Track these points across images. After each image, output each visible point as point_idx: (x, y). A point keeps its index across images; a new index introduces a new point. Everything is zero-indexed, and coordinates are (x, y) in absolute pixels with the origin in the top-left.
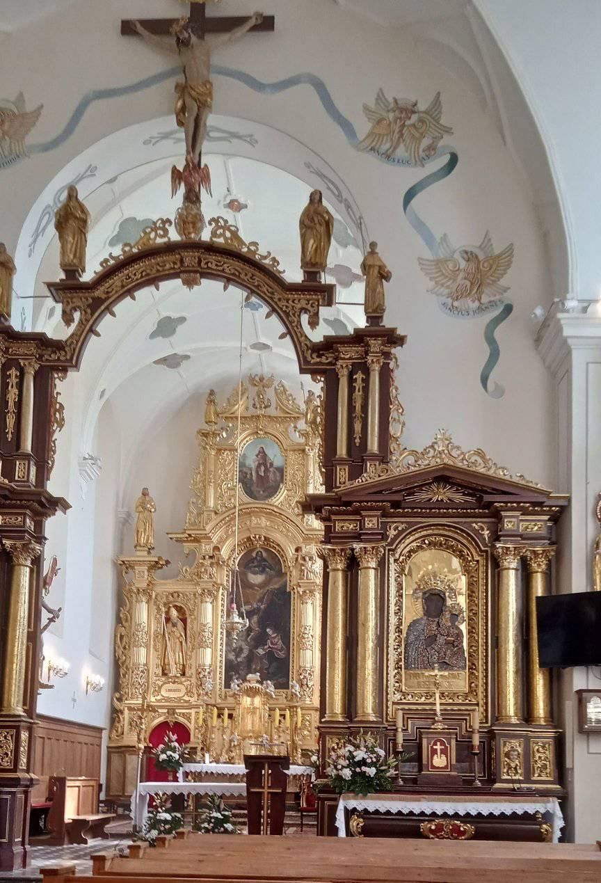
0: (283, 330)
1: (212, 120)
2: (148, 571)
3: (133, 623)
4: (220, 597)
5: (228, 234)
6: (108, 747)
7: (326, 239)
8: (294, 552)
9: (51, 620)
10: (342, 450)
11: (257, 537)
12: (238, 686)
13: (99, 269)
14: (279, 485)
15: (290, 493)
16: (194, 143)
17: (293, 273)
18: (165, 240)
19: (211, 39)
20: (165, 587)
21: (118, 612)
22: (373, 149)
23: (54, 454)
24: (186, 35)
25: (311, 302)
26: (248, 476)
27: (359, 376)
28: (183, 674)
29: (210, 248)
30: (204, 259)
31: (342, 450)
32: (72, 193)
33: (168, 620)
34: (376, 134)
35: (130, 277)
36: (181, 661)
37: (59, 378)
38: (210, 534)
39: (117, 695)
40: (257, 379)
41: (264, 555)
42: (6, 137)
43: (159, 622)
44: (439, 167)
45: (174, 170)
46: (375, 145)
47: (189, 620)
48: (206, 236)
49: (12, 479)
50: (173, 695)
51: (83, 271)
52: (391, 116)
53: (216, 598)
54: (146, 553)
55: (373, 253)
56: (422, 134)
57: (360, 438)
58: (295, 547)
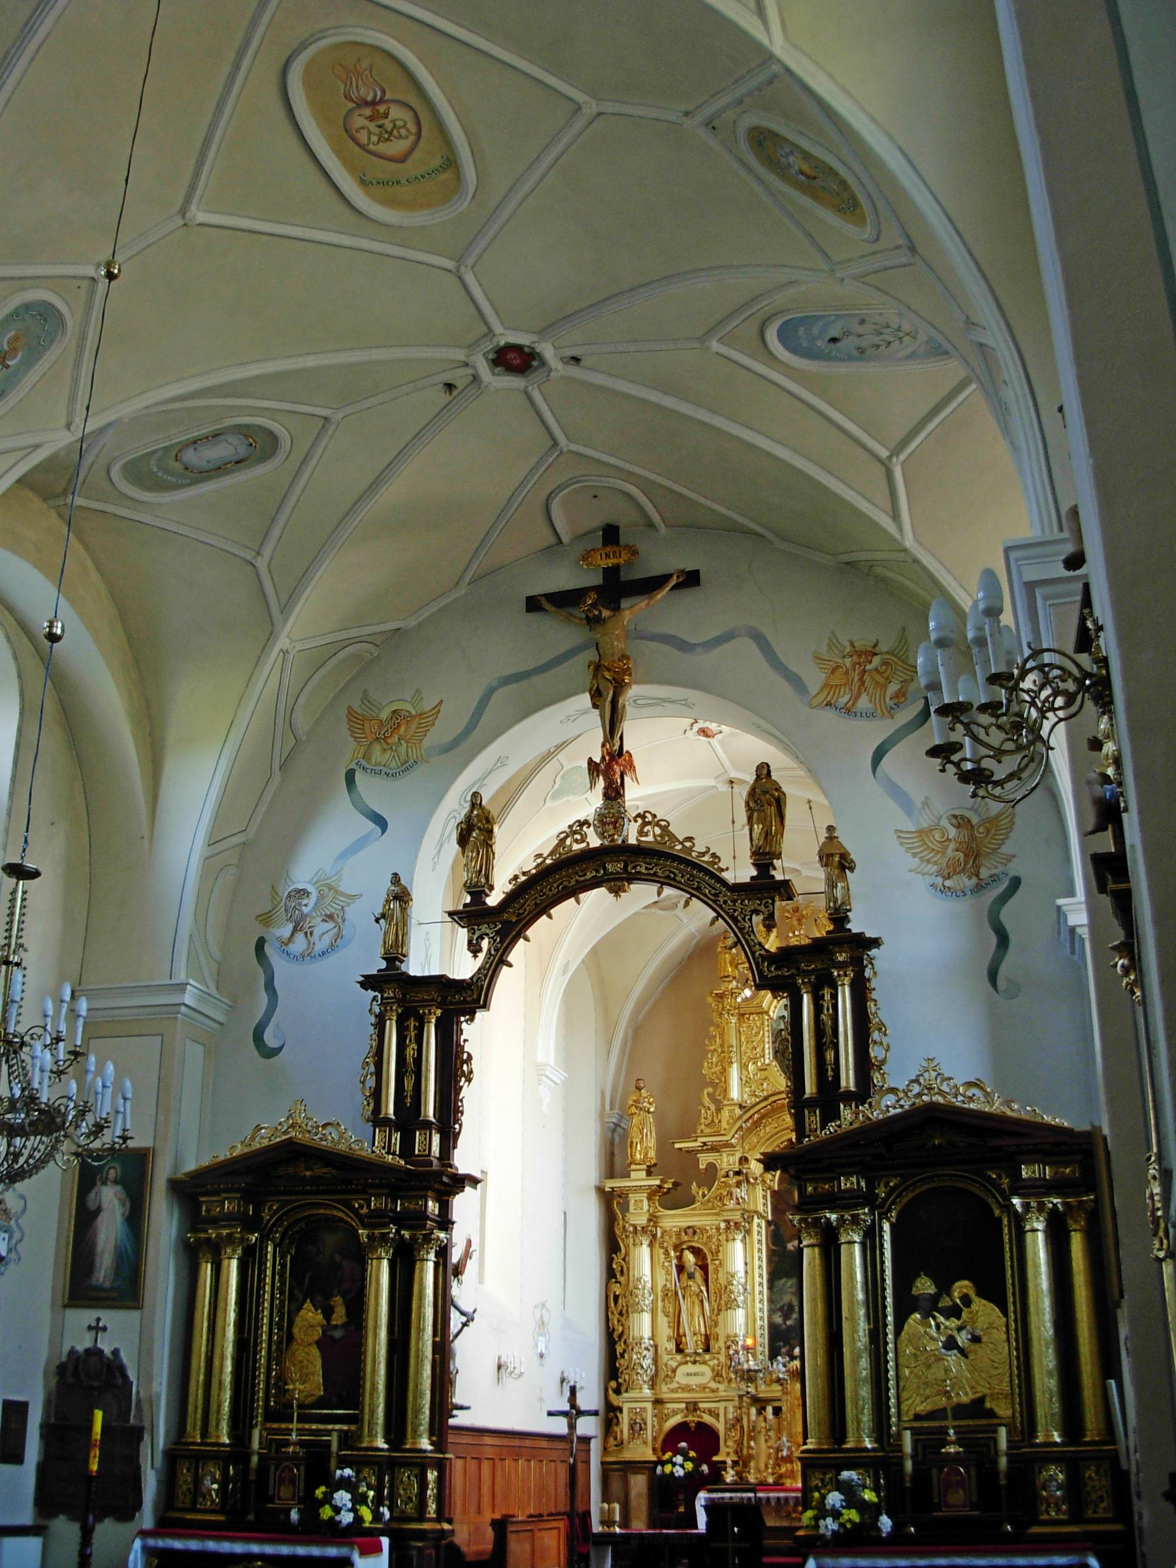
1: (634, 691)
2: (649, 1199)
3: (631, 1278)
4: (755, 1228)
5: (658, 831)
6: (603, 1463)
7: (778, 819)
9: (465, 1325)
10: (810, 1088)
12: (785, 1366)
13: (509, 888)
16: (612, 725)
17: (741, 871)
18: (583, 845)
20: (674, 1221)
21: (610, 1262)
22: (829, 704)
27: (412, 1023)
28: (707, 1350)
31: (810, 1088)
33: (681, 1268)
36: (703, 1329)
37: (466, 1021)
39: (613, 1384)
43: (668, 1273)
44: (915, 713)
45: (590, 761)
47: (711, 1268)
50: (693, 1381)
51: (491, 888)
52: (848, 661)
53: (748, 1232)
56: (887, 679)
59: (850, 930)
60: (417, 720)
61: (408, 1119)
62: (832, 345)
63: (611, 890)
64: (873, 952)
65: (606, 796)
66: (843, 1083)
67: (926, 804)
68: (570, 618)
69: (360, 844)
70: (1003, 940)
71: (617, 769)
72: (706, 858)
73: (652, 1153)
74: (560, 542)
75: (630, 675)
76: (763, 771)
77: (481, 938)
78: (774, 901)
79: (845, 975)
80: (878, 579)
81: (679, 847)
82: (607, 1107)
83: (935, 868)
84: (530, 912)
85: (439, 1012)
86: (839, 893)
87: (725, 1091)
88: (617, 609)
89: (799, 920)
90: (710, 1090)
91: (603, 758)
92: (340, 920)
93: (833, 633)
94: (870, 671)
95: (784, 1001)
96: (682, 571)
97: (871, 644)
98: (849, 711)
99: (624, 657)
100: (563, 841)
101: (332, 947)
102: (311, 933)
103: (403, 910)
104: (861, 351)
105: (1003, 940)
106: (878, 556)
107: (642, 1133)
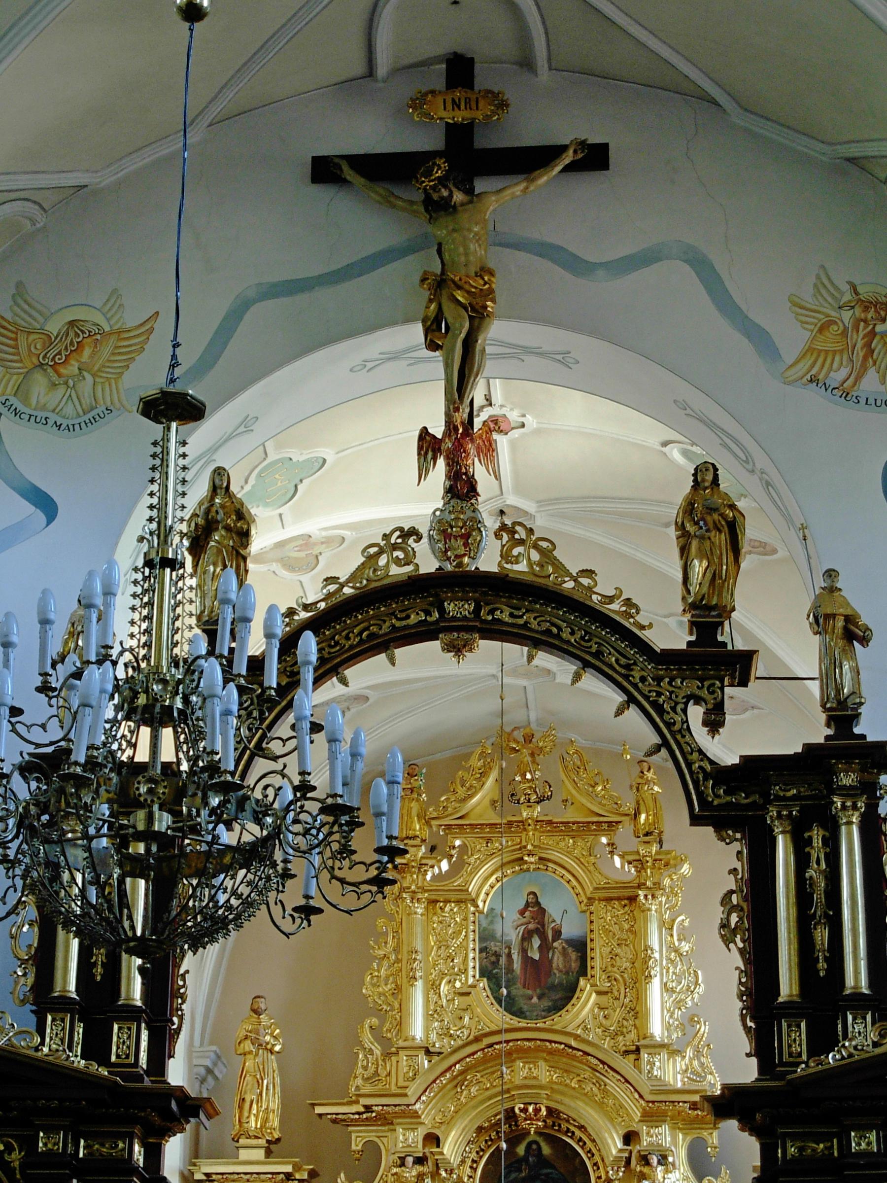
0: (619, 698)
1: (497, 332)
5: (535, 556)
7: (731, 558)
8: (620, 1145)
10: (788, 985)
11: (531, 1109)
14: (578, 981)
15: (604, 998)
17: (670, 632)
18: (410, 568)
23: (183, 1002)
24: (445, 193)
25: (706, 684)
26: (503, 961)
27: (817, 835)
30: (487, 604)
31: (788, 985)
34: (820, 351)
35: (337, 643)
38: (417, 1106)
40: (519, 735)
41: (546, 1150)
42: (85, 373)
45: (424, 434)
46: (819, 373)
48: (488, 560)
49: (104, 1060)
54: (260, 1154)
55: (832, 590)
57: (826, 959)
58: (622, 1132)
61: (98, 1003)
65: (452, 492)
66: (850, 981)
68: (388, 202)
73: (275, 1121)
74: (371, 72)
75: (493, 301)
79: (855, 807)
82: (197, 1041)
87: (401, 1025)
89: (532, 755)
90: (375, 1021)
93: (822, 267)
95: (736, 846)
98: (846, 395)
99: (484, 271)
100: (371, 559)
107: (259, 1084)
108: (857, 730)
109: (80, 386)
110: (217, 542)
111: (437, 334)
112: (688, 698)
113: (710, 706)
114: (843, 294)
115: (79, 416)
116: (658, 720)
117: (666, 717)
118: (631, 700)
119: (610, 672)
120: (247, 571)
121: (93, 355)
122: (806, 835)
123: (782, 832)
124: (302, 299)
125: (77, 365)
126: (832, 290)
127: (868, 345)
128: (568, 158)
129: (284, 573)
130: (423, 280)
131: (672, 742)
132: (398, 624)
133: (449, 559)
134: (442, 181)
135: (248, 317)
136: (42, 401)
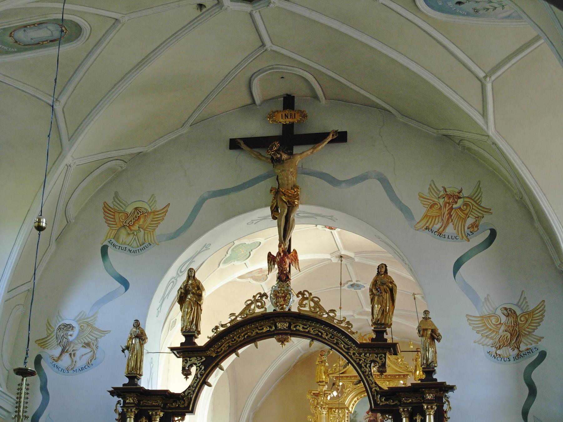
1: (301, 208)
5: (312, 304)
7: (391, 304)
13: (211, 334)
19: (297, 150)
24: (279, 156)
25: (379, 356)
29: (299, 317)
30: (294, 323)
32: (191, 275)
35: (235, 340)
45: (270, 254)
48: (294, 305)
52: (441, 201)
59: (436, 380)
60: (152, 216)
62: (458, 6)
63: (279, 340)
64: (450, 394)
65: (279, 278)
67: (487, 299)
68: (259, 157)
69: (110, 297)
70: (533, 391)
71: (288, 261)
72: (343, 325)
74: (254, 102)
75: (298, 199)
76: (382, 270)
77: (191, 366)
78: (385, 355)
79: (432, 408)
80: (464, 147)
81: (326, 316)
83: (491, 341)
84: (225, 351)
85: (162, 414)
86: (430, 355)
88: (291, 154)
91: (279, 254)
92: (94, 347)
94: (455, 209)
96: (336, 131)
97: (457, 191)
98: (440, 234)
99: (295, 187)
100: (248, 306)
101: (89, 365)
102: (74, 355)
103: (141, 345)
104: (476, 11)
105: (533, 391)
106: (466, 135)
108: (434, 377)
109: (139, 234)
110: (189, 299)
111: (276, 213)
112: (372, 361)
113: (380, 365)
114: (440, 192)
115: (138, 247)
116: (359, 370)
117: (363, 369)
118: (349, 362)
119: (341, 351)
120: (201, 310)
121: (145, 221)
122: (414, 418)
123: (405, 417)
124: (226, 197)
125: (138, 226)
126: (435, 189)
127: (449, 213)
128: (330, 138)
129: (254, 282)
130: (271, 191)
131: (364, 379)
132: (259, 332)
133: (278, 306)
134: (277, 151)
135: (204, 205)
136: (124, 241)
